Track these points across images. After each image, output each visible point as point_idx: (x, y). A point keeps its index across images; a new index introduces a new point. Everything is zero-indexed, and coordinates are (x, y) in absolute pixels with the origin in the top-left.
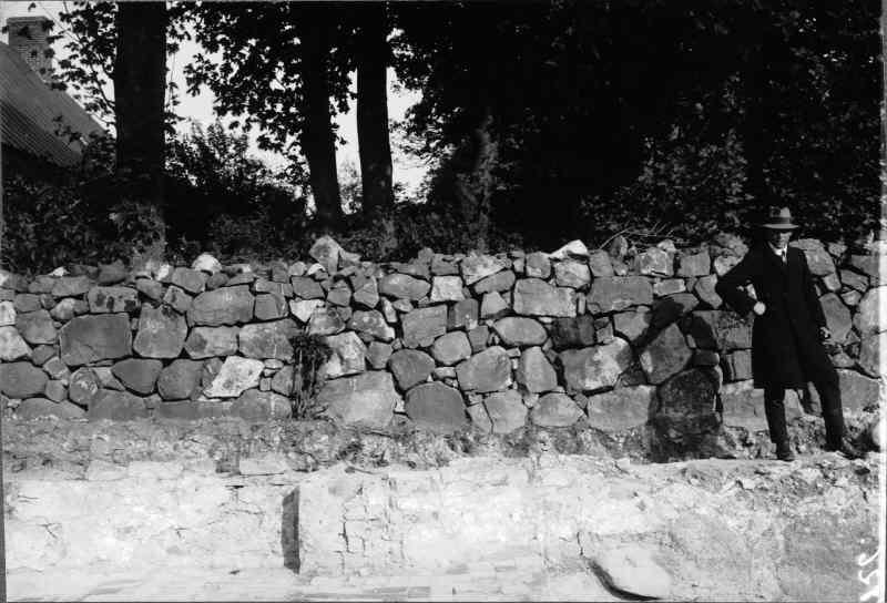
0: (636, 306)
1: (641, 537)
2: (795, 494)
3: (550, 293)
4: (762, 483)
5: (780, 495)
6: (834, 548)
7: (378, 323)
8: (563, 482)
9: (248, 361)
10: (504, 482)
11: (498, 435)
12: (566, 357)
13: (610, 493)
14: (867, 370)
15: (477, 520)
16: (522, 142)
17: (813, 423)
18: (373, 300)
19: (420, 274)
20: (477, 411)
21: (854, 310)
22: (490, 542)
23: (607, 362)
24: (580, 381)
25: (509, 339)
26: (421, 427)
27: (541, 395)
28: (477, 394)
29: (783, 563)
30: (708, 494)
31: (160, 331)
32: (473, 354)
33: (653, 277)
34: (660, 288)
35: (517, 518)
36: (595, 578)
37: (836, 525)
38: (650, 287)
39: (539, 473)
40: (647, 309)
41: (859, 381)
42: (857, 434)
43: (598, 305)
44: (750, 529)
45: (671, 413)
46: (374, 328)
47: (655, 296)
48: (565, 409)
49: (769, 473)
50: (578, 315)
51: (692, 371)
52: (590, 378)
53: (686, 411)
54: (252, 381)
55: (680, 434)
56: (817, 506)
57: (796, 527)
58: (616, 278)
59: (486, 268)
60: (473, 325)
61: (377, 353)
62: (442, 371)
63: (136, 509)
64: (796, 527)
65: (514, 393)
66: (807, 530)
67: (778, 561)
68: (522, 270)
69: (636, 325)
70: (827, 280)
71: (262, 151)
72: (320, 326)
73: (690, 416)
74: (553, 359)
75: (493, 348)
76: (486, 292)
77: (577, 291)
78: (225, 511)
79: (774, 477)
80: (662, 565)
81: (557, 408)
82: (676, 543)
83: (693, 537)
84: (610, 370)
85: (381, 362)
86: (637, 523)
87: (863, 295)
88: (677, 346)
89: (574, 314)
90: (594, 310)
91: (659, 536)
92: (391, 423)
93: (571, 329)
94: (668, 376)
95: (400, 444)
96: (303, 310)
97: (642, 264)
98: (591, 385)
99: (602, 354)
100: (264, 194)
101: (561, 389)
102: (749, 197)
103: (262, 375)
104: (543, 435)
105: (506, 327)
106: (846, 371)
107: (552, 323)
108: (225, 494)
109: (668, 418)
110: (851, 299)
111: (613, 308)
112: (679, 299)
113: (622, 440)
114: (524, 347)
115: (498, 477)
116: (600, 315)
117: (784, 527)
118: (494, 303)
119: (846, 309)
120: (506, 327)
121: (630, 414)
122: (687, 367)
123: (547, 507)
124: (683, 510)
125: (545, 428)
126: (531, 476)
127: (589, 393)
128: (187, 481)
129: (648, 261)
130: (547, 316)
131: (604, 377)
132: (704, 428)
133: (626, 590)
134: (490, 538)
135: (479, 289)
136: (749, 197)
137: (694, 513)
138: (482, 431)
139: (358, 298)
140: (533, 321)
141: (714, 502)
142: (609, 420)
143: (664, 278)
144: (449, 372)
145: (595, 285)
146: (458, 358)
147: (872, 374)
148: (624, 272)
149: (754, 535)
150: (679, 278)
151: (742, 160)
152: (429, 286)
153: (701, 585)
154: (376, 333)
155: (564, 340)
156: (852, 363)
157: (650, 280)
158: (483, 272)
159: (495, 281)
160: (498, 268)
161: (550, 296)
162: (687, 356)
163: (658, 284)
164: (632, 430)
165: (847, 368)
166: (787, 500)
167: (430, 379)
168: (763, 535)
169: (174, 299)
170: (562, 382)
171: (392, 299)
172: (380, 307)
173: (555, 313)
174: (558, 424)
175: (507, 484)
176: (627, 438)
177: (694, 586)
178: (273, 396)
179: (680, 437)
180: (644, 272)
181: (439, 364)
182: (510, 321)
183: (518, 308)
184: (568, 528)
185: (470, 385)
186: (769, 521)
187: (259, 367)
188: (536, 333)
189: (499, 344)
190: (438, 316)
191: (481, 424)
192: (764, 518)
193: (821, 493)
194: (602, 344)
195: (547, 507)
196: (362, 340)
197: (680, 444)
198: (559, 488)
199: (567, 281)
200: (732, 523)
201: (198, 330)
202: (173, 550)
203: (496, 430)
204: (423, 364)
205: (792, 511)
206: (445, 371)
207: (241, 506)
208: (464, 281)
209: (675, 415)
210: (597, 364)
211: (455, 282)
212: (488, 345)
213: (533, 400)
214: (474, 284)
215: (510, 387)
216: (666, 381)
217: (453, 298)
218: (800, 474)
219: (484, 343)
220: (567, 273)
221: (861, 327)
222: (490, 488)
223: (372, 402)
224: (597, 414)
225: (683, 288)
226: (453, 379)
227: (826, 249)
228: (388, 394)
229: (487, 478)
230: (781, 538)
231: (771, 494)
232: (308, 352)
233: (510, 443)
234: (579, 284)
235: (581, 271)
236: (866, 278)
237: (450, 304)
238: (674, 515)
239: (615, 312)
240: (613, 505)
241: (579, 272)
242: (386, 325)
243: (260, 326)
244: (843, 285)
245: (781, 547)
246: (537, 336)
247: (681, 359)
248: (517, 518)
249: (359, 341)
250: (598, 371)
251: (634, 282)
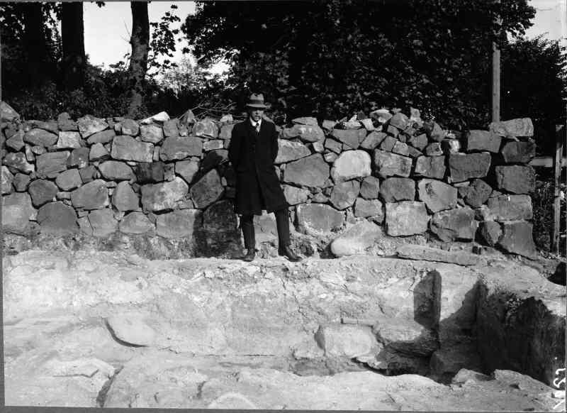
0: (191, 157)
1: (140, 306)
2: (241, 282)
3: (136, 145)
4: (219, 274)
5: (231, 282)
6: (261, 318)
7: (21, 160)
11: (95, 237)
12: (146, 189)
13: (121, 277)
14: (335, 205)
15: (34, 291)
16: (395, 44)
17: (299, 238)
19: (51, 129)
20: (83, 222)
21: (331, 164)
22: (42, 306)
23: (173, 192)
24: (151, 205)
25: (107, 175)
26: (44, 232)
27: (127, 213)
28: (85, 210)
29: (230, 326)
30: (183, 280)
32: (83, 184)
33: (204, 138)
34: (208, 146)
35: (59, 290)
36: (108, 331)
37: (264, 302)
38: (200, 144)
39: (74, 262)
40: (198, 160)
41: (329, 211)
42: (325, 246)
43: (166, 155)
44: (208, 303)
45: (209, 228)
46: (17, 164)
47: (203, 151)
48: (141, 222)
49: (225, 268)
50: (154, 161)
51: (223, 201)
52: (158, 203)
53: (218, 227)
55: (215, 242)
56: (252, 291)
57: (238, 303)
58: (179, 138)
59: (95, 127)
60: (83, 165)
61: (19, 181)
62: (61, 194)
64: (238, 303)
66: (246, 306)
67: (227, 325)
68: (119, 130)
69: (194, 167)
70: (315, 145)
73: (221, 230)
74: (136, 190)
75: (97, 181)
76: (94, 143)
77: (156, 145)
79: (227, 270)
80: (149, 325)
81: (135, 222)
82: (160, 311)
83: (170, 306)
84: (170, 198)
85: (22, 187)
86: (137, 297)
88: (214, 184)
89: (151, 161)
90: (164, 158)
91: (151, 305)
92: (26, 227)
93: (147, 170)
94: (208, 203)
95: (29, 241)
97: (197, 129)
98: (158, 207)
99: (165, 187)
101: (140, 209)
102: (293, 88)
104: (126, 239)
105: (105, 167)
106: (321, 205)
107: (137, 166)
109: (207, 231)
110: (329, 157)
111: (176, 157)
112: (219, 153)
113: (177, 244)
114: (118, 181)
115: (50, 263)
116: (167, 162)
117: (231, 303)
118: (98, 151)
119: (326, 164)
121: (182, 227)
122: (220, 199)
123: (80, 284)
124: (166, 290)
125: (126, 234)
126: (70, 264)
129: (200, 127)
130: (133, 161)
131: (167, 203)
132: (228, 239)
133: (122, 339)
134: (41, 303)
136: (293, 88)
137: (172, 292)
138: (87, 234)
139: (10, 143)
140: (124, 164)
141: (186, 285)
142: (169, 231)
144: (65, 195)
145: (165, 142)
146: (72, 186)
147: (338, 208)
148: (185, 134)
149: (212, 307)
150: (220, 139)
151: (286, 64)
152: (326, 146)
153: (173, 339)
154: (19, 167)
155: (144, 178)
156: (326, 199)
157: (202, 139)
158: (94, 130)
159: (100, 136)
160: (103, 128)
161: (136, 148)
162: (221, 191)
163: (207, 142)
164: (183, 237)
165: (323, 203)
166: (234, 286)
167: (55, 199)
168: (218, 307)
170: (141, 205)
171: (32, 145)
172: (23, 150)
173: (137, 159)
174: (137, 232)
175: (53, 268)
176: (180, 243)
177: (169, 339)
179: (215, 244)
180: (198, 134)
181: (61, 190)
182: (108, 163)
183: (114, 155)
184: (92, 298)
185: (79, 205)
186: (221, 299)
188: (124, 171)
189: (101, 178)
190: (60, 158)
191: (86, 230)
192: (219, 297)
193: (256, 283)
194: (167, 181)
195: (80, 284)
196: (11, 172)
197: (214, 248)
198: (88, 272)
199: (149, 138)
200: (196, 299)
203: (94, 234)
204: (49, 189)
205: (237, 293)
206: (63, 195)
208: (81, 136)
209: (211, 229)
211: (73, 135)
212: (94, 179)
214: (88, 137)
215: (107, 207)
216: (208, 207)
217: (72, 146)
218: (246, 269)
219: (91, 177)
220: (148, 133)
221: (335, 176)
222: (43, 270)
224: (162, 227)
225: (221, 146)
226: (68, 200)
227: (320, 125)
228: (27, 208)
229: (42, 264)
230: (229, 310)
231: (225, 281)
233: (103, 243)
234: (156, 140)
235: (157, 132)
236: (341, 145)
238: (159, 292)
239: (177, 160)
240: (122, 285)
241: (156, 132)
242: (26, 163)
244: (325, 148)
245: (229, 315)
246: (125, 174)
247: (217, 193)
248: (59, 290)
249: (8, 172)
250: (162, 199)
251: (190, 140)
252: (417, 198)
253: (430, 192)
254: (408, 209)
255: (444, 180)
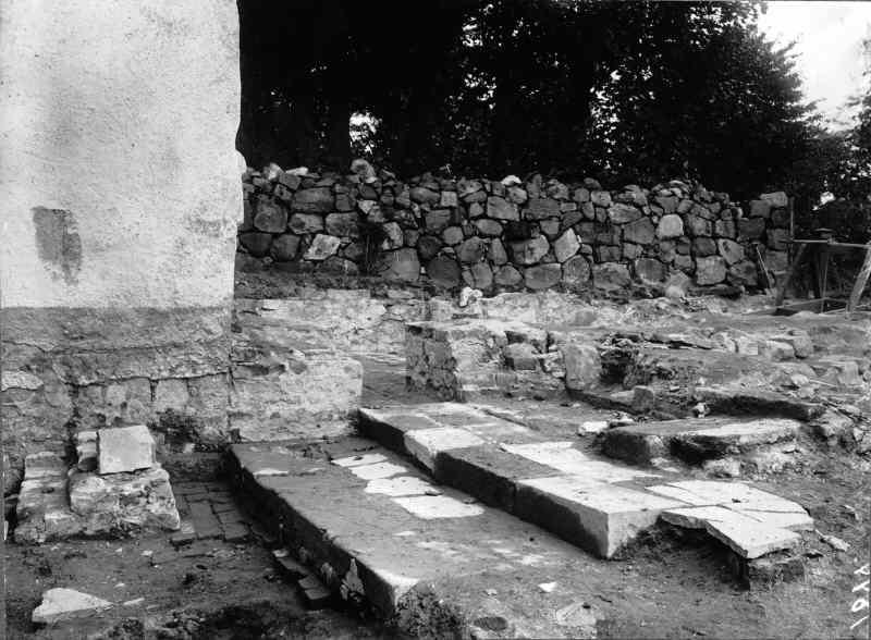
8: (556, 306)
9: (332, 238)
10: (527, 306)
18: (407, 202)
21: (656, 226)
25: (484, 231)
31: (273, 214)
32: (465, 240)
50: (521, 220)
54: (333, 250)
63: (334, 317)
65: (486, 265)
71: (29, 216)
72: (377, 217)
78: (384, 319)
87: (659, 218)
96: (366, 206)
98: (528, 261)
99: (533, 244)
100: (501, 36)
103: (340, 246)
108: (382, 310)
110: (655, 220)
116: (533, 221)
118: (476, 210)
120: (482, 224)
126: (541, 303)
127: (527, 266)
128: (363, 301)
135: (468, 200)
143: (565, 201)
146: (457, 242)
155: (516, 234)
158: (471, 190)
163: (563, 205)
169: (282, 194)
178: (346, 261)
183: (490, 214)
187: (338, 242)
198: (554, 310)
201: (298, 215)
202: (354, 342)
207: (392, 316)
210: (531, 249)
213: (496, 269)
222: (519, 309)
223: (406, 266)
232: (369, 235)
234: (521, 201)
235: (522, 193)
237: (451, 208)
243: (340, 215)
250: (532, 253)
252: (718, 253)
253: (727, 249)
254: (713, 263)
255: (735, 240)
